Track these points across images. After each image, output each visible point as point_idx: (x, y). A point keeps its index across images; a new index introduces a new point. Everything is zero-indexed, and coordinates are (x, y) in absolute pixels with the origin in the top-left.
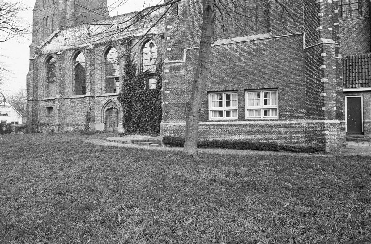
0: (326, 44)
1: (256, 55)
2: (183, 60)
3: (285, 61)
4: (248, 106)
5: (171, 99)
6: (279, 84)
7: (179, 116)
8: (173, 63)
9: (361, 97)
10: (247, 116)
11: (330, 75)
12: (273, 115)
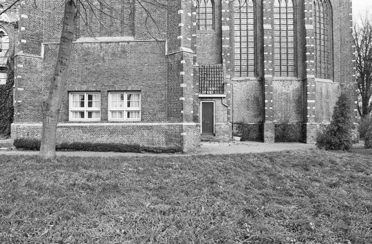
0: (185, 53)
1: (120, 57)
2: (40, 55)
3: (148, 65)
4: (110, 108)
5: (25, 97)
6: (142, 87)
7: (34, 116)
8: (28, 57)
9: (213, 103)
10: (110, 118)
11: (189, 81)
12: (136, 118)
